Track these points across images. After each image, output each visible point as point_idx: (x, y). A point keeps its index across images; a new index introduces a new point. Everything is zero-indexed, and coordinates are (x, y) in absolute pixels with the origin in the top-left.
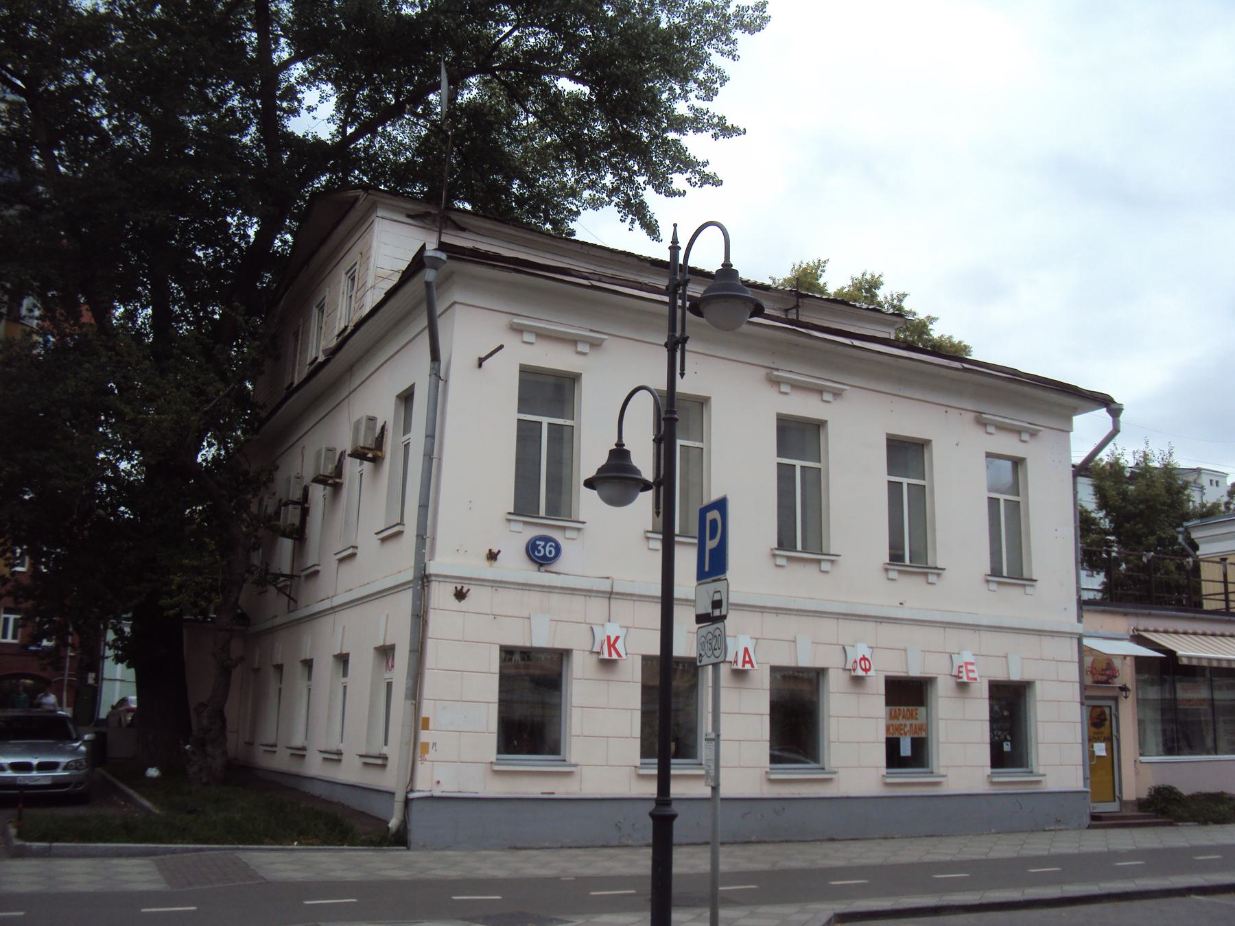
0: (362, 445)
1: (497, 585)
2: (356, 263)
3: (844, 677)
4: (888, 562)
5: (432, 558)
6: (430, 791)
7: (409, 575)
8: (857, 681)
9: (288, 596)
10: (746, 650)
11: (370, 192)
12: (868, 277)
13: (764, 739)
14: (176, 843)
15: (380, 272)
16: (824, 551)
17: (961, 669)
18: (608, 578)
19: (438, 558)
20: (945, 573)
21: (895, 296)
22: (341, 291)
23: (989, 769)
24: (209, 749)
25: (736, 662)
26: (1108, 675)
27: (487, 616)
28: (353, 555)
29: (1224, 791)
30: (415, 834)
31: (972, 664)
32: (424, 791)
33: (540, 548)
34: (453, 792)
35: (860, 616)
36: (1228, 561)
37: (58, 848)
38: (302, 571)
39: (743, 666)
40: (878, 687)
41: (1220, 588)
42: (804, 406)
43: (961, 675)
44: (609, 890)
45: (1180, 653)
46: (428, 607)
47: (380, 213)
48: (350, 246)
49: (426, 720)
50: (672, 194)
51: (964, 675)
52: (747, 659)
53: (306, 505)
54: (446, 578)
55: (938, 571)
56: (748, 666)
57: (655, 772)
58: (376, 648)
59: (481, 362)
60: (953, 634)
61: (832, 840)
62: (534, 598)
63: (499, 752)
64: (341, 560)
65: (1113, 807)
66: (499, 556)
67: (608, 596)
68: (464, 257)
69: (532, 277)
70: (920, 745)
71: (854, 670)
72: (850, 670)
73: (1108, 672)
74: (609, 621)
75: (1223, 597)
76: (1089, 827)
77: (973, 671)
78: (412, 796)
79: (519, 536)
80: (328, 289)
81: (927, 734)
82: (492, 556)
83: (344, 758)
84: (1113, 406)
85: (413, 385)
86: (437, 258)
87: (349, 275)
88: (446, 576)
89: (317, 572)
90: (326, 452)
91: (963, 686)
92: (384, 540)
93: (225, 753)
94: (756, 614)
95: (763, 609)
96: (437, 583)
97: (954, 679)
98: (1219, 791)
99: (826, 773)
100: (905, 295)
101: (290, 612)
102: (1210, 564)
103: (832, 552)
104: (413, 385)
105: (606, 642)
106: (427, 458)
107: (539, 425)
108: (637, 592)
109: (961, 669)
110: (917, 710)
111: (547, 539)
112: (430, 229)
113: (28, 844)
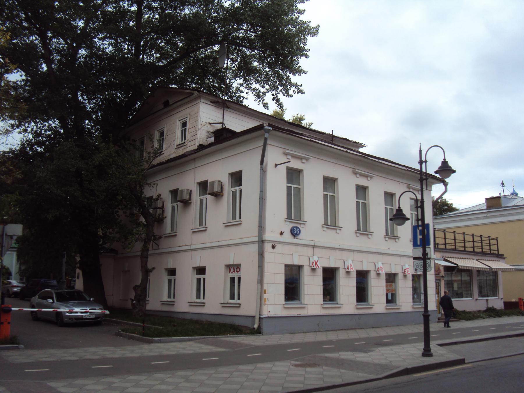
0: (217, 191)
1: (283, 243)
3: (344, 271)
4: (385, 235)
6: (267, 315)
8: (314, 270)
10: (351, 264)
11: (200, 92)
12: (299, 116)
13: (283, 294)
14: (195, 336)
15: (202, 123)
16: (368, 230)
17: (405, 271)
18: (313, 241)
20: (400, 239)
21: (308, 124)
22: (177, 127)
23: (412, 303)
25: (348, 269)
28: (206, 230)
29: (466, 310)
30: (264, 329)
31: (408, 269)
32: (265, 315)
33: (295, 230)
34: (274, 315)
35: (379, 253)
36: (465, 234)
37: (163, 339)
38: (164, 234)
39: (351, 270)
40: (384, 277)
41: (480, 244)
42: (363, 182)
43: (405, 272)
44: (294, 349)
45: (459, 265)
49: (265, 291)
50: (289, 96)
51: (406, 272)
52: (351, 268)
54: (269, 241)
55: (398, 237)
56: (352, 270)
60: (344, 253)
61: (373, 327)
62: (293, 248)
63: (285, 301)
66: (283, 234)
67: (313, 247)
68: (275, 129)
69: (298, 138)
70: (393, 295)
71: (378, 271)
72: (376, 271)
74: (314, 255)
75: (481, 247)
76: (438, 322)
77: (409, 271)
78: (262, 316)
79: (287, 228)
81: (395, 292)
82: (282, 233)
84: (445, 183)
86: (269, 129)
88: (269, 241)
89: (176, 235)
91: (348, 273)
94: (371, 254)
95: (354, 251)
97: (403, 273)
99: (338, 305)
100: (312, 124)
102: (439, 232)
103: (371, 232)
105: (314, 262)
107: (290, 187)
108: (321, 246)
109: (405, 271)
110: (392, 284)
111: (297, 227)
112: (218, 107)
113: (154, 338)
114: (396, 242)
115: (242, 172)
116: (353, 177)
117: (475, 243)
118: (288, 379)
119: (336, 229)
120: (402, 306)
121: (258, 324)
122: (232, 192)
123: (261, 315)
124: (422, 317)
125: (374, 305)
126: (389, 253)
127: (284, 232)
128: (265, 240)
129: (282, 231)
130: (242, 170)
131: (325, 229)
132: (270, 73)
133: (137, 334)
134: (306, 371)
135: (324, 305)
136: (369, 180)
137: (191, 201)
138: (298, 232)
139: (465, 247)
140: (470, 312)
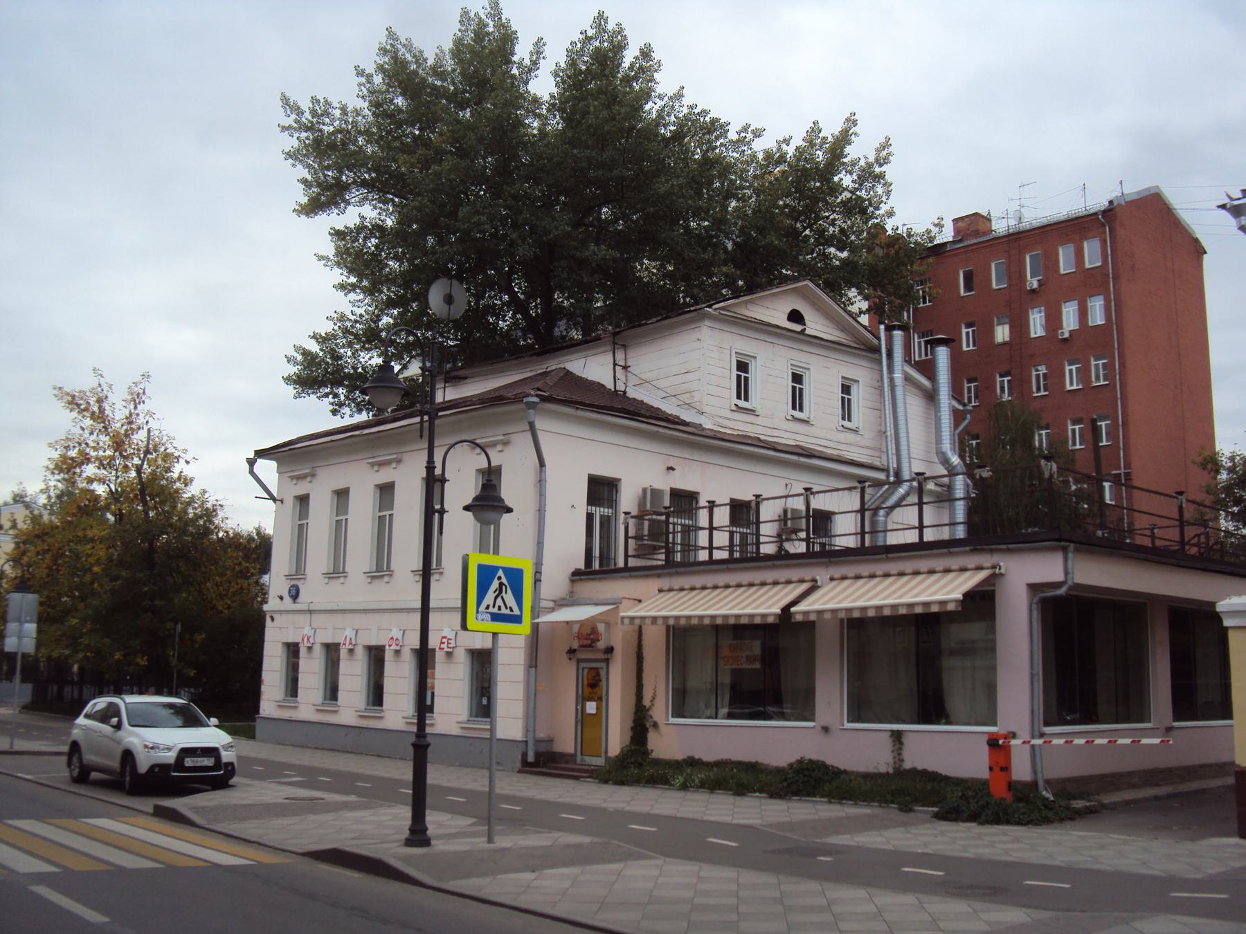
26: (592, 639)
29: (760, 761)
57: (416, 721)
65: (600, 761)
68: (692, 309)
73: (592, 637)
76: (520, 772)
98: (754, 760)
115: (394, 485)
117: (715, 552)
118: (697, 900)
124: (411, 751)
126: (402, 607)
130: (394, 482)
132: (229, 550)
133: (1104, 374)
134: (738, 897)
139: (753, 544)
140: (838, 773)
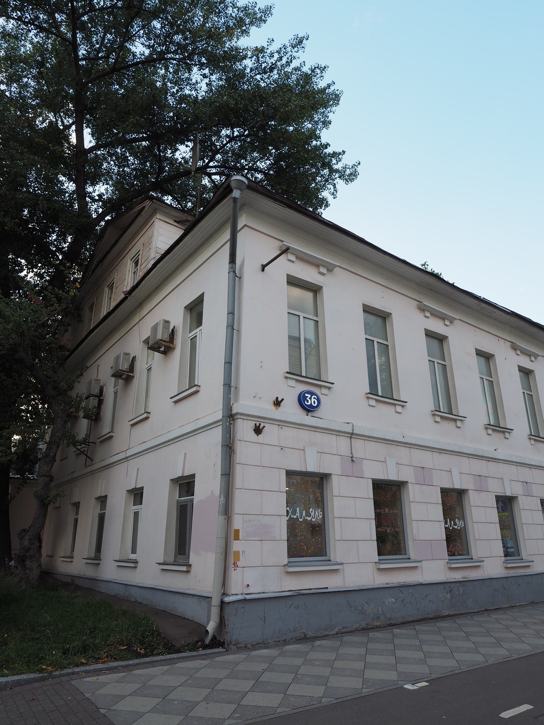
1: (282, 424)
2: (140, 251)
5: (236, 400)
7: (219, 415)
9: (86, 455)
19: (241, 402)
20: (513, 433)
24: (28, 563)
27: (277, 447)
28: (147, 418)
33: (308, 399)
46: (234, 441)
47: (158, 216)
48: (134, 244)
49: (237, 532)
53: (101, 398)
58: (172, 480)
59: (263, 267)
62: (305, 434)
64: (133, 425)
78: (227, 599)
80: (116, 274)
82: (278, 403)
83: (139, 565)
85: (203, 295)
87: (133, 260)
90: (123, 355)
92: (176, 402)
93: (40, 565)
96: (242, 420)
101: (86, 467)
104: (203, 295)
106: (230, 328)
111: (312, 394)
114: (506, 438)
116: (419, 316)
119: (395, 405)
120: (533, 561)
121: (218, 621)
122: (190, 340)
123: (227, 595)
125: (483, 561)
127: (283, 400)
128: (237, 414)
129: (277, 398)
131: (373, 403)
135: (380, 564)
136: (447, 326)
137: (133, 373)
138: (314, 403)
